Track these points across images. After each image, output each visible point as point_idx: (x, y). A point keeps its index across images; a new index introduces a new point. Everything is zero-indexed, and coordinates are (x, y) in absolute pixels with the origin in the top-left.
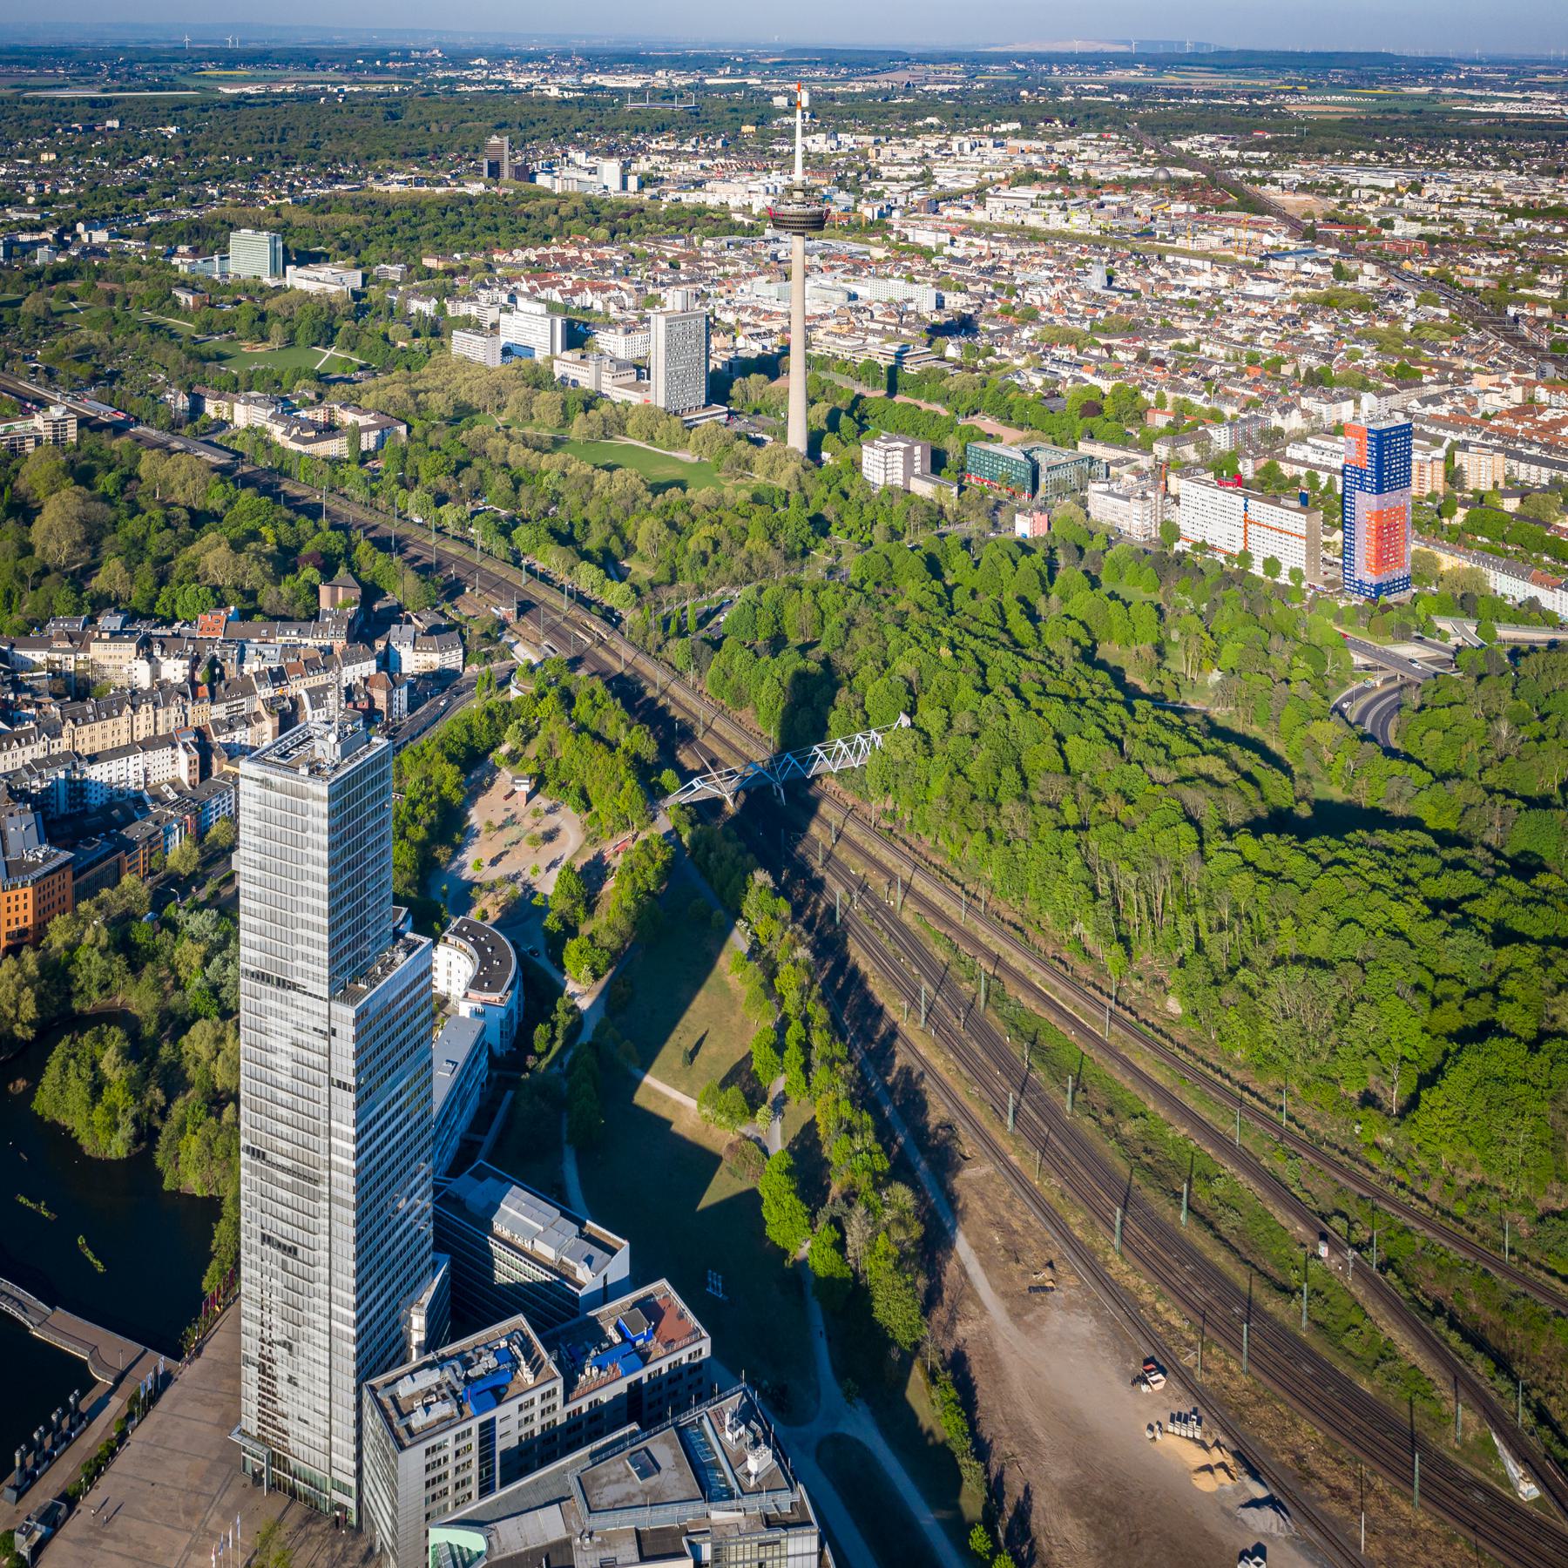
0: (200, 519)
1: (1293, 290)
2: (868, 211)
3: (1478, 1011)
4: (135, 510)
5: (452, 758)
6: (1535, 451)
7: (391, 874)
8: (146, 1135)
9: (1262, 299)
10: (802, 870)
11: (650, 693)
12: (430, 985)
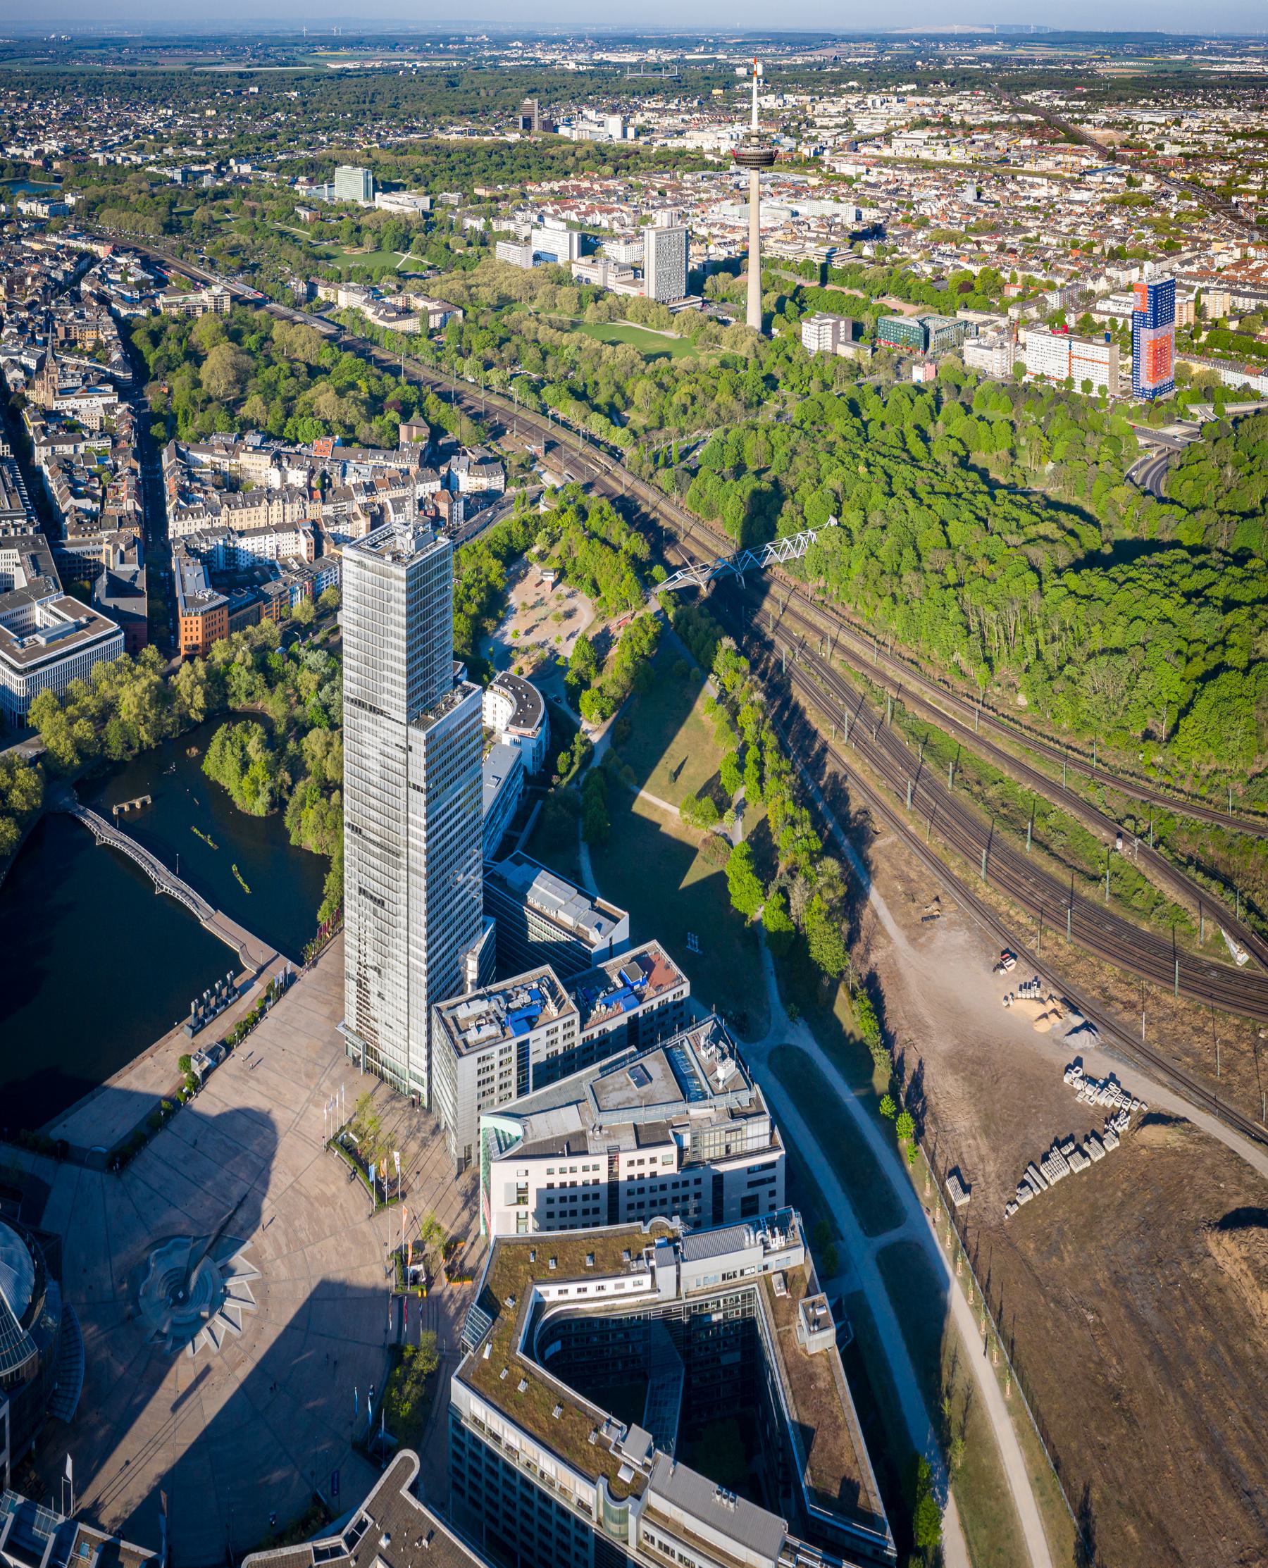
0: (314, 372)
1: (1100, 196)
2: (806, 151)
3: (1214, 658)
4: (270, 362)
5: (496, 555)
6: (1248, 289)
7: (451, 638)
8: (278, 803)
9: (1081, 203)
10: (758, 635)
11: (644, 509)
12: (480, 720)
